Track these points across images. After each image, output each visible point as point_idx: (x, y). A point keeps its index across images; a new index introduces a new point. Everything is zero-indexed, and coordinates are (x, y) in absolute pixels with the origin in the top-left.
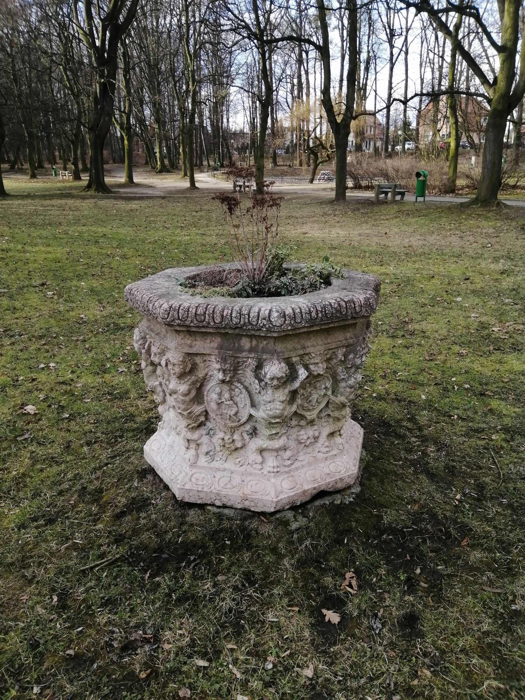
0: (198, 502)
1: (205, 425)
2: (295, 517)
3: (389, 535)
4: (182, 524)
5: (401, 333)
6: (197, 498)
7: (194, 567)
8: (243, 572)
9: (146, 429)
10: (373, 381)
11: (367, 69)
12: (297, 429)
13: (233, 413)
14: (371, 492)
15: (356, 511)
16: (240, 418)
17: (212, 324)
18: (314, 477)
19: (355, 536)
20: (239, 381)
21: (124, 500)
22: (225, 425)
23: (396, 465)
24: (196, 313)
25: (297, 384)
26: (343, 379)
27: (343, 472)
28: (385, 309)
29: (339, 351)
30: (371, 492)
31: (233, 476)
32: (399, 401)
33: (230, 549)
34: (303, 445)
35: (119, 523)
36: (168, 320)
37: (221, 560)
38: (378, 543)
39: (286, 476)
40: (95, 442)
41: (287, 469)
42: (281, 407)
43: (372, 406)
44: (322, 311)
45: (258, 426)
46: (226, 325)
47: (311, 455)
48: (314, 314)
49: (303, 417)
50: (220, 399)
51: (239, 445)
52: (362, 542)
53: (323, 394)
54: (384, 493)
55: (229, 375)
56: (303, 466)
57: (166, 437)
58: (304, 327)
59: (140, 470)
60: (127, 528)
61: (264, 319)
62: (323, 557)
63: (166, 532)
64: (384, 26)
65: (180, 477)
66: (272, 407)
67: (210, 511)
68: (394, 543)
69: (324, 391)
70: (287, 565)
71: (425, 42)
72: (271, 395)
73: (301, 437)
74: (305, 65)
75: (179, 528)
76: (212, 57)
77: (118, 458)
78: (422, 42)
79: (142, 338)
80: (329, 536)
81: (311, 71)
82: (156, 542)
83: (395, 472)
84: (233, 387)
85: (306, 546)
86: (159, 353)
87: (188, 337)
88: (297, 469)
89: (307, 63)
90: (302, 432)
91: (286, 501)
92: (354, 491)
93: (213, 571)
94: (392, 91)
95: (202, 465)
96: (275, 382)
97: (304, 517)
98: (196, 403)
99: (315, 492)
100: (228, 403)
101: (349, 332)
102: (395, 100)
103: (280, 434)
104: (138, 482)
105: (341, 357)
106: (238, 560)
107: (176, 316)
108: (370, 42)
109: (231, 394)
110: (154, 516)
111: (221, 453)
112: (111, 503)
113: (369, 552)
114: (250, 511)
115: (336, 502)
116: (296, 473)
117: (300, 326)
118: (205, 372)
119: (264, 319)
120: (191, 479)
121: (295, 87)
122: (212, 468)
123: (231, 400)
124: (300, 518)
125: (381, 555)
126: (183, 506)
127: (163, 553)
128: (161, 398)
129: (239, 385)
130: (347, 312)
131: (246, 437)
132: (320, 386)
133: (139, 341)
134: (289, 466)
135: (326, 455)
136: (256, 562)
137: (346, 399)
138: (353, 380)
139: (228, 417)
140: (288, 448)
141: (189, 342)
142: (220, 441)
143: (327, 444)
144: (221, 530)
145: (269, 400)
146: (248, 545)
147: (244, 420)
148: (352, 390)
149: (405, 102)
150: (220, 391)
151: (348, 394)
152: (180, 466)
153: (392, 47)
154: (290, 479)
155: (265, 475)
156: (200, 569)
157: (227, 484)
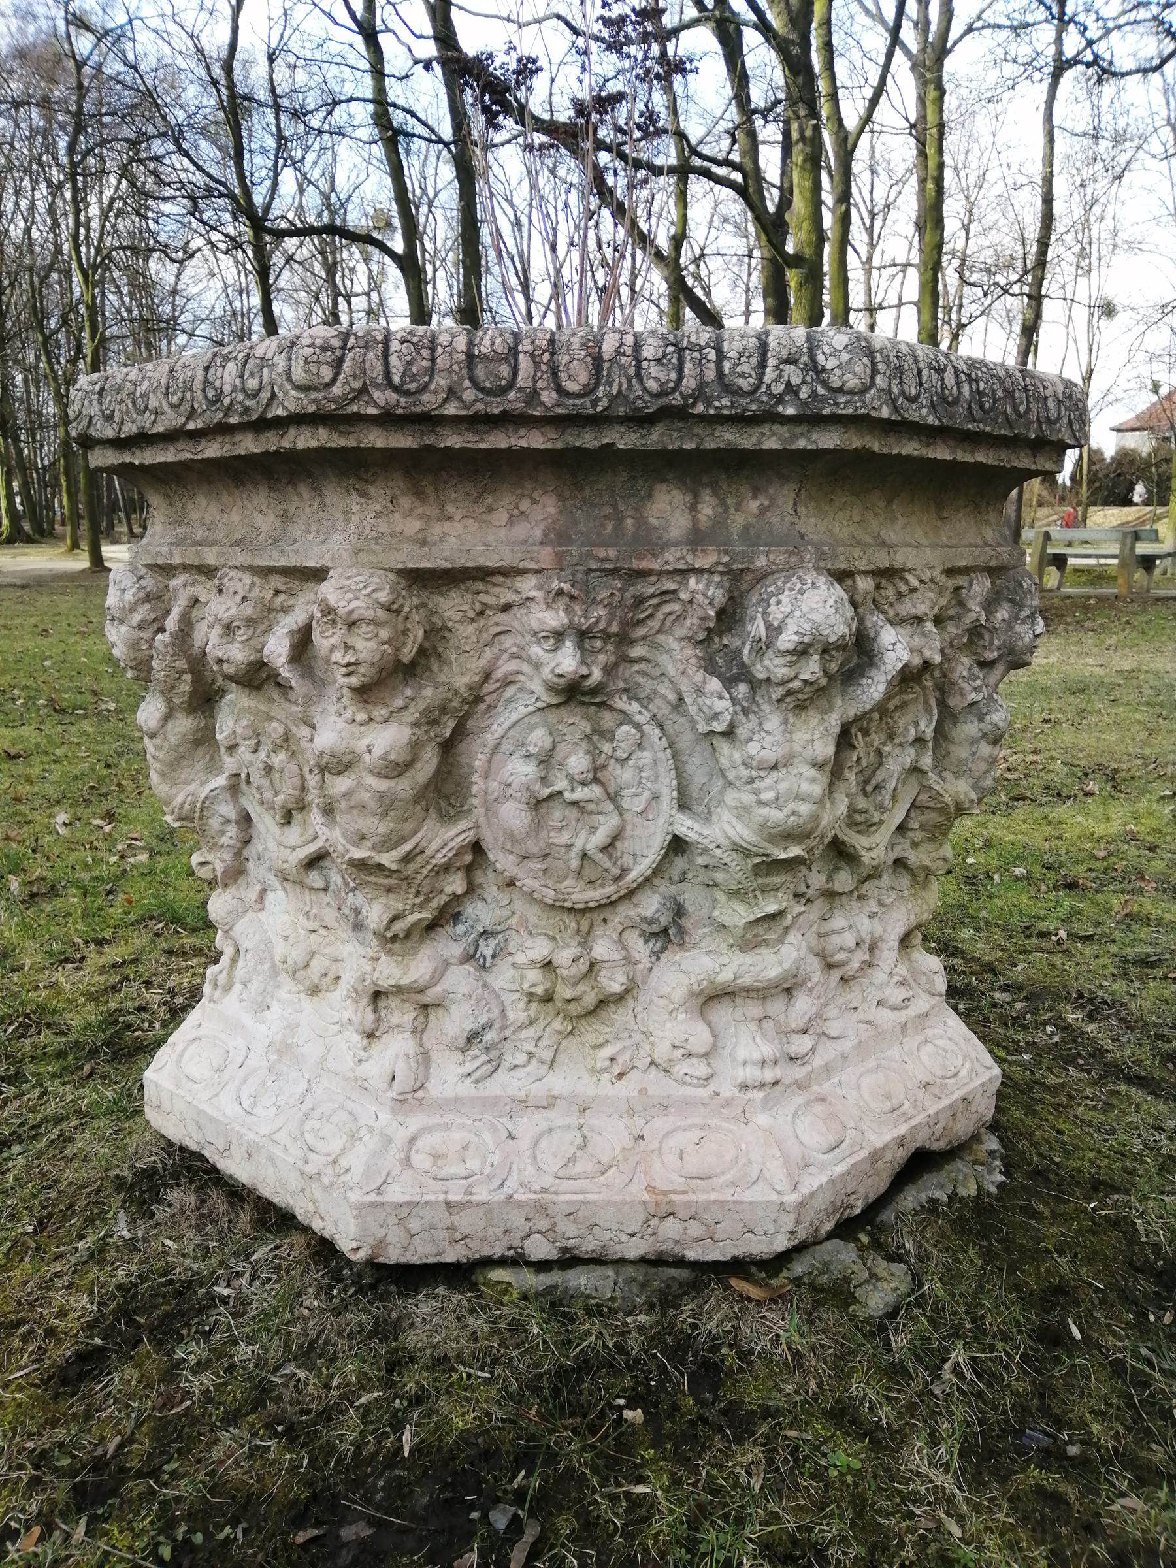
0: (450, 1257)
1: (456, 917)
4: (395, 1364)
9: (108, 1043)
12: (818, 908)
13: (601, 837)
16: (627, 861)
17: (548, 397)
18: (888, 1097)
21: (81, 1302)
24: (470, 356)
27: (964, 1073)
31: (593, 1120)
33: (656, 1444)
35: (79, 1408)
36: (336, 390)
39: (800, 1099)
46: (613, 399)
50: (544, 780)
51: (614, 982)
55: (602, 658)
57: (247, 1019)
59: (128, 1174)
60: (128, 1425)
61: (790, 360)
63: (327, 1415)
65: (356, 1160)
66: (783, 787)
67: (506, 1288)
72: (778, 737)
73: (836, 940)
75: (388, 1384)
76: (131, 295)
77: (16, 1149)
79: (147, 598)
82: (294, 1469)
84: (608, 719)
86: (250, 622)
87: (406, 502)
88: (828, 1069)
91: (822, 1202)
95: (449, 1092)
96: (811, 669)
99: (902, 1155)
100: (580, 794)
104: (132, 1223)
106: (714, 1490)
107: (377, 371)
109: (594, 752)
110: (243, 1351)
111: (530, 1032)
112: (23, 1321)
114: (681, 1262)
118: (483, 663)
119: (790, 360)
120: (407, 1162)
122: (494, 1102)
123: (596, 780)
126: (373, 1287)
127: (343, 1517)
128: (227, 856)
131: (640, 949)
133: (133, 608)
135: (902, 1016)
139: (575, 863)
141: (413, 526)
143: (903, 970)
144: (585, 1365)
145: (771, 756)
147: (641, 869)
150: (548, 743)
152: (345, 1116)
153: (529, 300)
154: (818, 1108)
155: (728, 1103)
157: (572, 1159)
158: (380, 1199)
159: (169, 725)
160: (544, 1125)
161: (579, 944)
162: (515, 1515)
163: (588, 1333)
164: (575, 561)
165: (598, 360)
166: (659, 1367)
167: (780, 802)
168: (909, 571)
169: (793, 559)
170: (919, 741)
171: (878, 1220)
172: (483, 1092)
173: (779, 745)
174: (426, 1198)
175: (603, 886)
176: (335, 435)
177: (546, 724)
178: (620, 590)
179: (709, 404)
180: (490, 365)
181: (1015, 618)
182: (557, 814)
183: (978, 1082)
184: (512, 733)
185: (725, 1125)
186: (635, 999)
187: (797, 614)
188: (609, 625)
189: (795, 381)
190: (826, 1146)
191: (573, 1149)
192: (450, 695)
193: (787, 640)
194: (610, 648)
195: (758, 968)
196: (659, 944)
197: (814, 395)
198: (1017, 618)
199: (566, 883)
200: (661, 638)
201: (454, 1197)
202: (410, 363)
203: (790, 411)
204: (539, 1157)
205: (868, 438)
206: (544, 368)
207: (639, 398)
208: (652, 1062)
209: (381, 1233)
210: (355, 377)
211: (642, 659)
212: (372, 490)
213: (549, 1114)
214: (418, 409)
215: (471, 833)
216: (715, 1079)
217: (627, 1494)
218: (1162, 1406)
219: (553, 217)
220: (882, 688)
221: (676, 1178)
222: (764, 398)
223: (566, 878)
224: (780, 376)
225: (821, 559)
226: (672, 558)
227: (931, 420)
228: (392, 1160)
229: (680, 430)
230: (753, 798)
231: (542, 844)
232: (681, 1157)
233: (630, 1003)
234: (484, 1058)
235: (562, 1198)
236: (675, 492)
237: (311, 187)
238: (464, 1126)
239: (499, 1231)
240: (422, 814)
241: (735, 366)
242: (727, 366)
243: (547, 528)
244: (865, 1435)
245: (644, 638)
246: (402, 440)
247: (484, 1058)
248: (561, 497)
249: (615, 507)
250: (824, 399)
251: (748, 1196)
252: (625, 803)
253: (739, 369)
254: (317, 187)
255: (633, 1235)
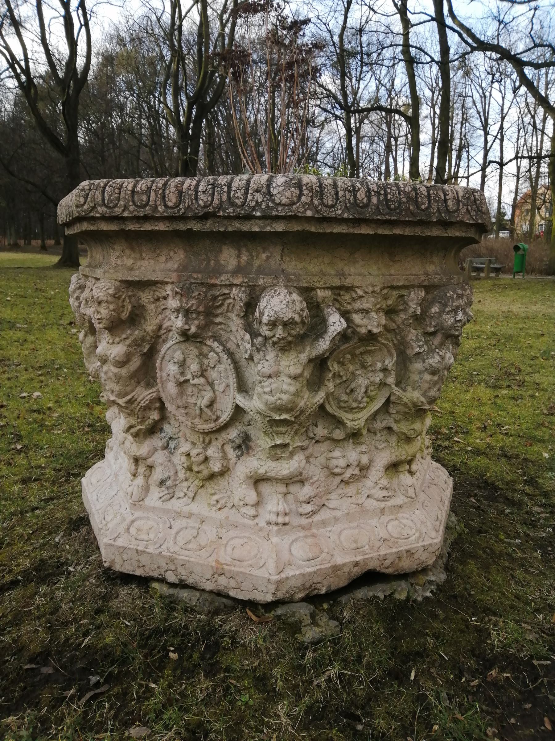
0: (138, 573)
2: (313, 616)
3: (503, 670)
4: (99, 611)
5: (505, 384)
6: (135, 564)
7: (88, 701)
8: (188, 723)
10: (467, 433)
11: (459, 157)
12: (324, 447)
13: (205, 402)
14: (465, 583)
15: (436, 617)
16: (219, 413)
17: (161, 209)
18: (356, 542)
19: (433, 665)
20: (216, 338)
22: (193, 429)
23: (509, 544)
24: (133, 191)
25: (324, 344)
26: (418, 354)
27: (413, 538)
28: (480, 361)
29: (412, 295)
30: (465, 583)
31: (204, 527)
32: (509, 458)
33: (174, 670)
34: (338, 479)
36: (85, 207)
37: (148, 689)
38: (479, 686)
39: (302, 534)
40: (35, 480)
41: (304, 521)
42: (292, 389)
43: (465, 461)
44: (378, 193)
45: (252, 432)
47: (353, 500)
48: (361, 195)
49: (339, 423)
50: (182, 374)
51: (216, 467)
52: (447, 681)
53: (377, 380)
54: (490, 588)
55: (196, 322)
56: (336, 519)
58: (340, 221)
61: (258, 191)
62: (363, 708)
64: (479, 113)
66: (274, 386)
68: (513, 687)
69: (381, 375)
70: (283, 716)
71: (522, 130)
73: (334, 462)
74: (394, 153)
75: (93, 618)
78: (519, 131)
80: (380, 662)
81: (400, 159)
83: (509, 555)
84: (205, 349)
85: (329, 680)
87: (128, 252)
88: (324, 523)
89: (396, 151)
90: (337, 453)
91: (299, 583)
92: (433, 578)
93: (127, 714)
94: (486, 179)
95: (152, 505)
96: (279, 332)
97: (332, 618)
98: (142, 384)
99: (357, 571)
100: (196, 381)
101: (432, 262)
102: (491, 162)
103: (291, 448)
105: (414, 307)
106: (183, 695)
107: (99, 199)
108: (463, 130)
109: (201, 364)
110: (60, 593)
111: (185, 484)
113: (461, 705)
114: (228, 597)
115: (397, 596)
116: (322, 531)
117: (330, 213)
118: (157, 321)
119: (258, 191)
120: (128, 530)
121: (383, 176)
122: (168, 511)
123: (202, 375)
124: (323, 619)
125: (488, 713)
126: (114, 579)
127: (46, 663)
129: (216, 344)
130: (429, 206)
131: (231, 454)
132: (373, 365)
134: (307, 515)
135: (382, 505)
136: (219, 704)
137: (424, 395)
138: (437, 358)
139: (198, 412)
140: (307, 479)
141: (129, 262)
142: (184, 459)
143: (384, 482)
144: (166, 631)
145: (267, 371)
146: (211, 665)
147: (225, 417)
148: (436, 378)
149: (501, 164)
151: (426, 385)
153: (486, 134)
154: (310, 540)
155: (261, 529)
156: (100, 707)
157: (189, 542)
158: (113, 543)
159: (87, 339)
160: (184, 525)
161: (203, 448)
162: (99, 681)
163: (176, 618)
164: (185, 278)
165: (180, 192)
166: (196, 638)
167: (273, 392)
168: (358, 287)
169: (274, 281)
170: (385, 370)
171: (339, 599)
172: (165, 507)
173: (271, 366)
174: (130, 546)
175: (210, 423)
176: (89, 225)
177: (181, 349)
178: (204, 292)
179: (225, 212)
180: (140, 195)
181: (442, 312)
182: (190, 389)
183: (421, 544)
184: (168, 352)
185: (257, 539)
186: (230, 476)
187: (269, 307)
188: (198, 307)
189: (260, 200)
190: (305, 558)
191: (191, 537)
192: (145, 334)
193: (265, 319)
194: (201, 317)
195: (278, 469)
196: (240, 453)
197: (268, 206)
198: (444, 311)
199: (196, 420)
200: (229, 314)
201: (140, 548)
202: (111, 195)
203: (258, 214)
204: (178, 538)
205: (306, 225)
206: (159, 196)
207: (196, 208)
208: (233, 506)
209: (113, 557)
210: (91, 201)
211: (220, 323)
212: (115, 247)
213: (189, 521)
214: (113, 214)
215: (155, 394)
216: (259, 517)
217: (147, 686)
218: (430, 722)
219: (503, 92)
220: (328, 343)
221: (229, 559)
222: (247, 208)
223: (196, 418)
224: (253, 198)
225: (288, 281)
226: (224, 279)
227: (346, 215)
228: (122, 529)
229: (218, 222)
230: (262, 390)
231: (184, 402)
232: (233, 550)
233: (227, 477)
234: (166, 492)
235: (180, 557)
236: (231, 249)
237: (383, 88)
238: (154, 519)
239: (156, 566)
240: (135, 384)
241: (235, 194)
242: (232, 193)
243: (180, 264)
244: (267, 692)
245: (222, 314)
246: (113, 227)
247: (166, 492)
248: (185, 251)
249: (207, 255)
250: (272, 208)
251: (256, 573)
252: (216, 387)
253: (236, 195)
254: (385, 87)
255: (208, 580)
